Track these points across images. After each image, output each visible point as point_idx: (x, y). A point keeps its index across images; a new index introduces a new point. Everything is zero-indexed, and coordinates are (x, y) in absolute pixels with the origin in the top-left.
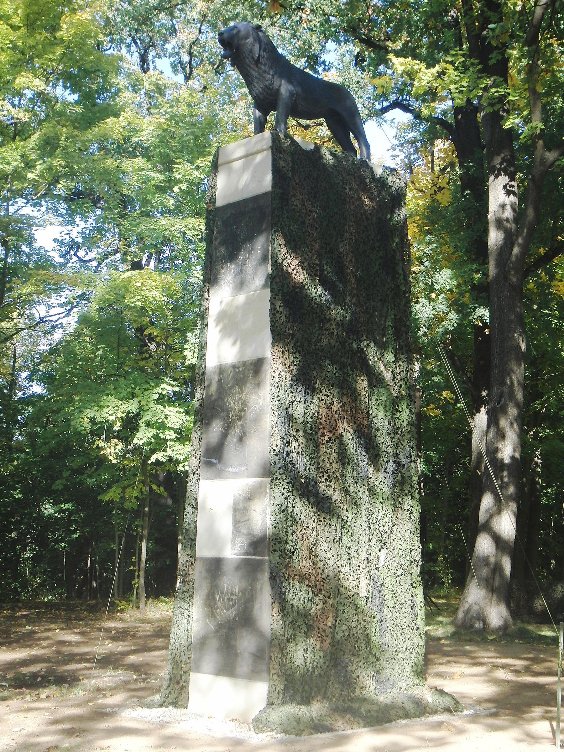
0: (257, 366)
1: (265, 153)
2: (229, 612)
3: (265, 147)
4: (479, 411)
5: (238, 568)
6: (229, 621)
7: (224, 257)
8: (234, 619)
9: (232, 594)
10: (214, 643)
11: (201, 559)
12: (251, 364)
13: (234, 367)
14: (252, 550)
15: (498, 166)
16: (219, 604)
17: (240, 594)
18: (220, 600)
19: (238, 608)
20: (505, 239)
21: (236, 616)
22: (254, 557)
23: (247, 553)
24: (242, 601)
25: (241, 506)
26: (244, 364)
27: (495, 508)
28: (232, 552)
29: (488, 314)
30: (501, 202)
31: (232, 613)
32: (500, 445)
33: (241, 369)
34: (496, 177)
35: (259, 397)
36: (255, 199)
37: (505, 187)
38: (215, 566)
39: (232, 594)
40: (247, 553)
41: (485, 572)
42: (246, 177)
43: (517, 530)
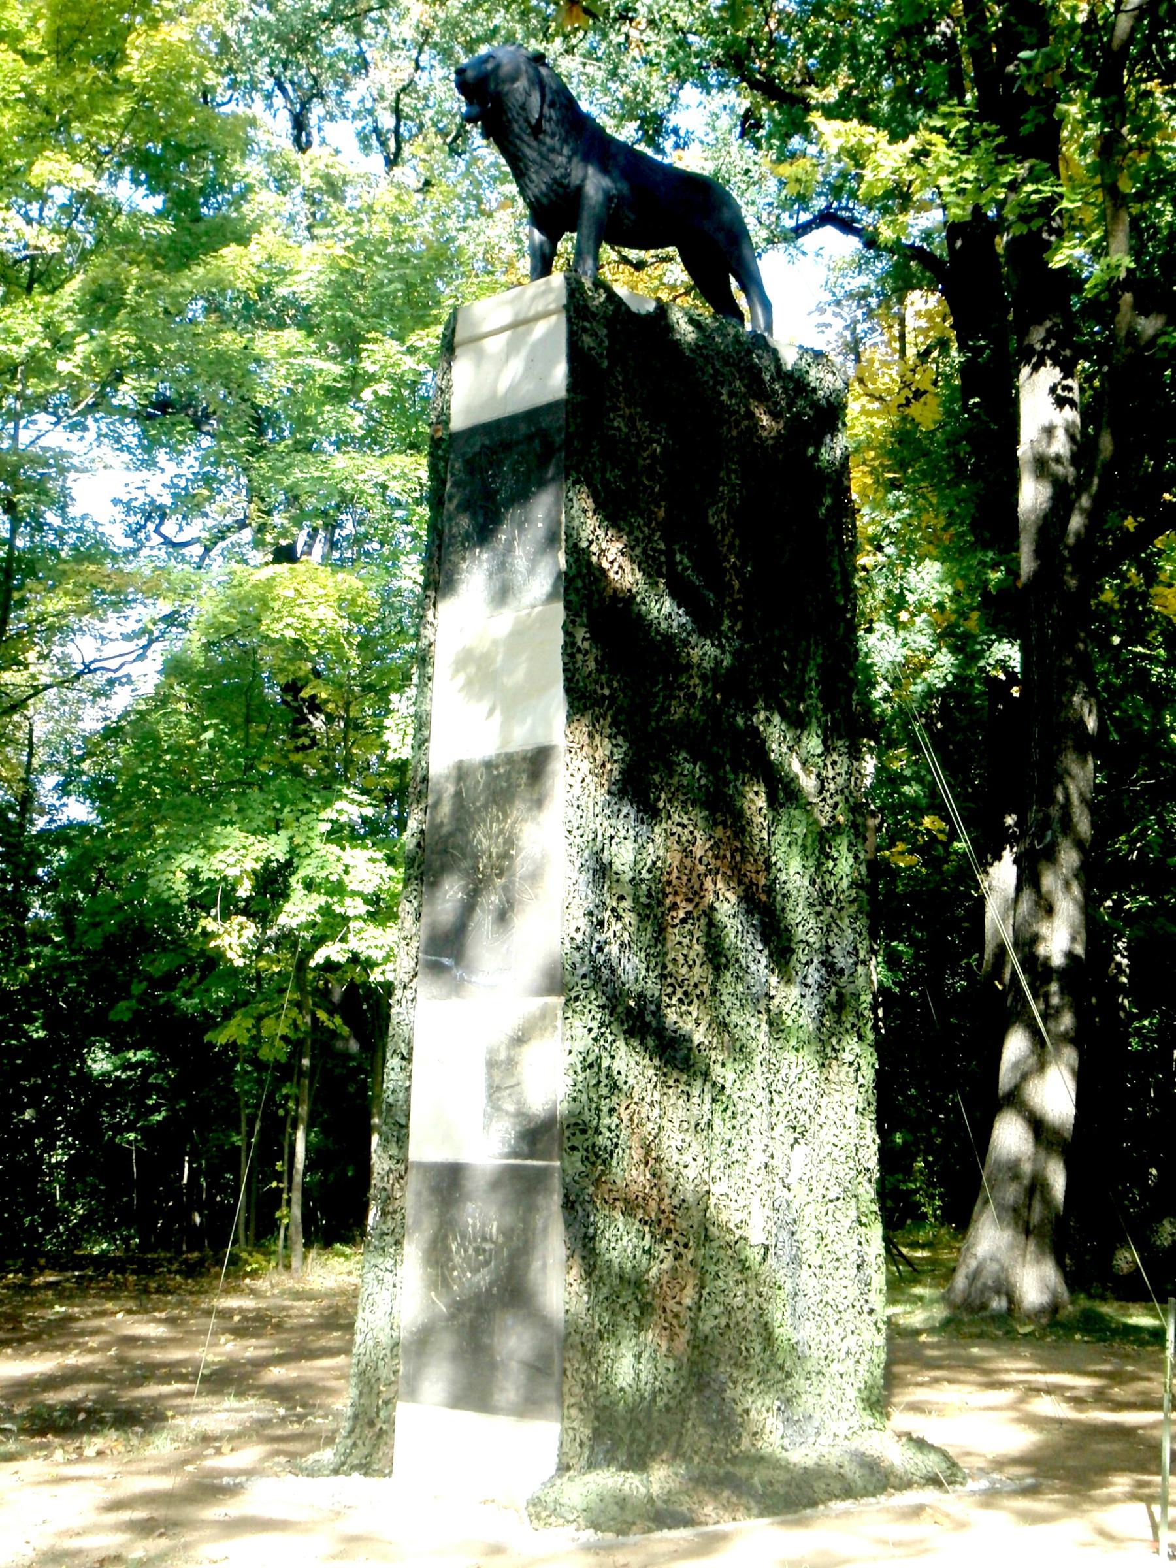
0: (537, 762)
2: (478, 1276)
3: (552, 307)
4: (999, 858)
6: (478, 1296)
7: (467, 536)
8: (489, 1290)
9: (484, 1239)
10: (446, 1342)
11: (420, 1165)
12: (524, 759)
14: (525, 1148)
15: (1038, 347)
16: (457, 1260)
17: (501, 1240)
18: (458, 1252)
21: (491, 1284)
22: (529, 1162)
23: (515, 1154)
25: (502, 1056)
26: (509, 759)
27: (1033, 1060)
28: (485, 1148)
32: (1044, 929)
34: (1036, 368)
36: (532, 415)
37: (1053, 390)
38: (449, 1181)
39: (484, 1239)
40: (515, 1154)
41: (1012, 1193)
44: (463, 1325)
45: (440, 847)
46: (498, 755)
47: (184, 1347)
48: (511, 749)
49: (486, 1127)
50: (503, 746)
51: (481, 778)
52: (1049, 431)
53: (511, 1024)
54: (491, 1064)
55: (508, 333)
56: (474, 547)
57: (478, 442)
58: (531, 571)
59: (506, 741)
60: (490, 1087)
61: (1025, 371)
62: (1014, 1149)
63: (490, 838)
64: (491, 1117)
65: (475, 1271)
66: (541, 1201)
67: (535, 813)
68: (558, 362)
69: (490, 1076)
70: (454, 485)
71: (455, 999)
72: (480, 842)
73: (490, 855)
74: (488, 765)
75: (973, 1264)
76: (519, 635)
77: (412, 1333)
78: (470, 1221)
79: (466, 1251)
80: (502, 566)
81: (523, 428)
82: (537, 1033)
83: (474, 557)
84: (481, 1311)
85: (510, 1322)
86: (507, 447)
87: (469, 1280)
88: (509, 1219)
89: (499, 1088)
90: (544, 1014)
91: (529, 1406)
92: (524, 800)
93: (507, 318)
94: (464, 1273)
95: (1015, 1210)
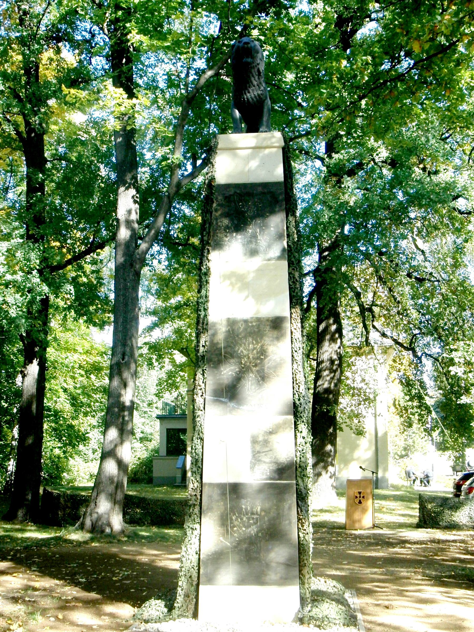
0: (276, 323)
1: (274, 150)
3: (277, 145)
4: (32, 362)
7: (227, 227)
9: (253, 514)
11: (210, 485)
12: (268, 320)
14: (277, 476)
15: (129, 181)
20: (131, 236)
21: (258, 532)
22: (278, 482)
25: (261, 438)
26: (259, 320)
27: (118, 440)
29: (73, 289)
30: (128, 208)
32: (123, 392)
33: (254, 324)
34: (127, 189)
36: (265, 185)
37: (133, 197)
38: (234, 490)
39: (253, 514)
41: (111, 489)
42: (254, 164)
45: (217, 352)
49: (252, 468)
51: (242, 327)
52: (129, 212)
53: (268, 426)
54: (254, 441)
55: (250, 151)
56: (233, 232)
57: (232, 191)
58: (269, 246)
60: (253, 452)
61: (122, 189)
62: (111, 472)
63: (248, 350)
64: (255, 464)
66: (287, 496)
67: (276, 342)
70: (218, 205)
72: (242, 352)
73: (249, 358)
74: (246, 321)
75: (95, 516)
76: (260, 271)
77: (208, 555)
78: (243, 507)
81: (260, 189)
82: (281, 430)
83: (232, 237)
85: (270, 547)
86: (250, 195)
87: (243, 531)
89: (259, 452)
90: (285, 423)
91: (284, 581)
92: (268, 337)
93: (253, 145)
95: (111, 495)
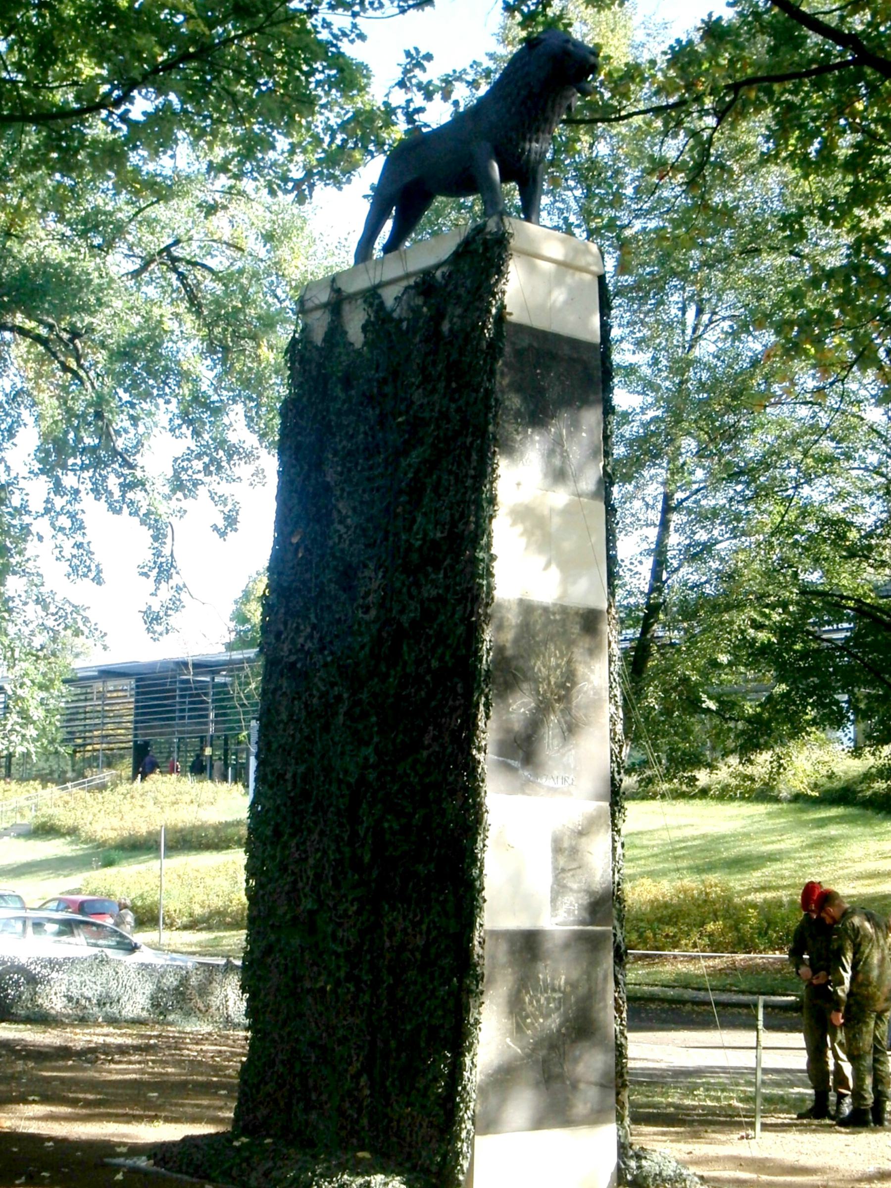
2: (549, 1021)
5: (567, 946)
6: (550, 1037)
7: (518, 414)
8: (559, 1031)
10: (530, 1075)
12: (577, 613)
13: (546, 610)
14: (586, 915)
16: (530, 1009)
17: (568, 989)
18: (531, 1003)
19: (566, 1012)
23: (582, 923)
24: (573, 999)
26: (564, 610)
28: (558, 919)
31: (554, 1022)
35: (592, 671)
38: (528, 945)
40: (582, 923)
43: (251, 894)
44: (537, 1061)
46: (555, 605)
47: (751, 970)
48: (567, 602)
50: (560, 598)
54: (557, 849)
59: (565, 594)
60: (555, 868)
65: (547, 1016)
68: (591, 313)
69: (555, 860)
71: (519, 798)
79: (538, 1001)
80: (556, 448)
81: (566, 350)
84: (553, 1047)
87: (541, 1024)
88: (575, 975)
89: (563, 870)
91: (595, 1118)
94: (536, 1020)
